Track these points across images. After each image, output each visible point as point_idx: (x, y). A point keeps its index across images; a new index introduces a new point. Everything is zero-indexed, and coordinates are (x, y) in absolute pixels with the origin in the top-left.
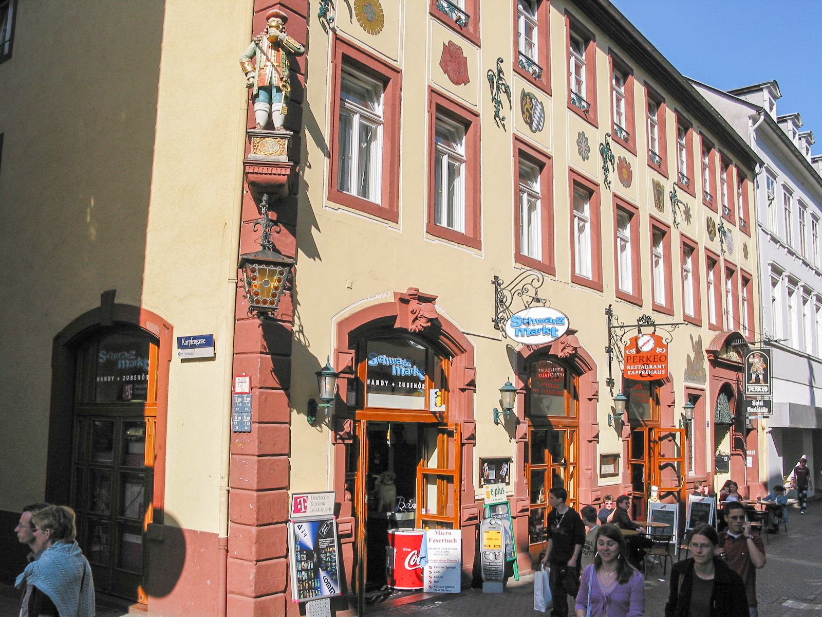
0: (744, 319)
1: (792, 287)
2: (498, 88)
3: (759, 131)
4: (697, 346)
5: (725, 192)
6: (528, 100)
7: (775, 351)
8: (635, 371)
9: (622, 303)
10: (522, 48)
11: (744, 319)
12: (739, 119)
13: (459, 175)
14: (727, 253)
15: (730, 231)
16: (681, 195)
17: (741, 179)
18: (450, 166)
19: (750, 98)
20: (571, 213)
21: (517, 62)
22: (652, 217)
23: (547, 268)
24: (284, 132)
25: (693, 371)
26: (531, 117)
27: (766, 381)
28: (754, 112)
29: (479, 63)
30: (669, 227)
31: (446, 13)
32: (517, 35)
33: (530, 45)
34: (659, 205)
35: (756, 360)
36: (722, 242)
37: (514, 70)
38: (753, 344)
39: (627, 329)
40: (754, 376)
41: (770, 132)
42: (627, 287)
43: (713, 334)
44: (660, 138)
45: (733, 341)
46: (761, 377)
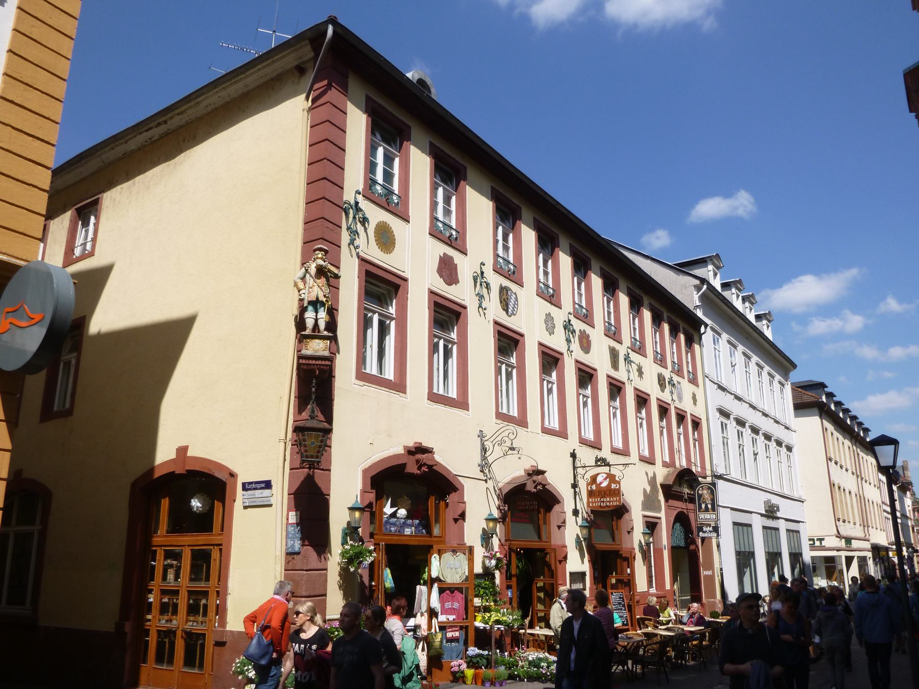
0: (695, 457)
1: (755, 436)
3: (703, 298)
4: (652, 481)
5: (690, 360)
7: (720, 483)
8: (597, 502)
9: (584, 447)
10: (440, 214)
11: (695, 457)
13: (452, 356)
14: (677, 402)
15: (679, 383)
16: (634, 356)
17: (690, 342)
18: (445, 347)
19: (699, 272)
20: (577, 391)
21: (496, 262)
22: (608, 376)
23: (521, 421)
24: (326, 333)
25: (649, 502)
26: (507, 305)
27: (713, 509)
28: (697, 282)
29: (465, 266)
30: (624, 383)
31: (441, 232)
32: (496, 242)
34: (615, 365)
35: (705, 492)
36: (672, 393)
37: (430, 234)
38: (705, 478)
40: (703, 506)
41: (714, 300)
42: (590, 435)
43: (665, 471)
45: (686, 477)
46: (709, 506)
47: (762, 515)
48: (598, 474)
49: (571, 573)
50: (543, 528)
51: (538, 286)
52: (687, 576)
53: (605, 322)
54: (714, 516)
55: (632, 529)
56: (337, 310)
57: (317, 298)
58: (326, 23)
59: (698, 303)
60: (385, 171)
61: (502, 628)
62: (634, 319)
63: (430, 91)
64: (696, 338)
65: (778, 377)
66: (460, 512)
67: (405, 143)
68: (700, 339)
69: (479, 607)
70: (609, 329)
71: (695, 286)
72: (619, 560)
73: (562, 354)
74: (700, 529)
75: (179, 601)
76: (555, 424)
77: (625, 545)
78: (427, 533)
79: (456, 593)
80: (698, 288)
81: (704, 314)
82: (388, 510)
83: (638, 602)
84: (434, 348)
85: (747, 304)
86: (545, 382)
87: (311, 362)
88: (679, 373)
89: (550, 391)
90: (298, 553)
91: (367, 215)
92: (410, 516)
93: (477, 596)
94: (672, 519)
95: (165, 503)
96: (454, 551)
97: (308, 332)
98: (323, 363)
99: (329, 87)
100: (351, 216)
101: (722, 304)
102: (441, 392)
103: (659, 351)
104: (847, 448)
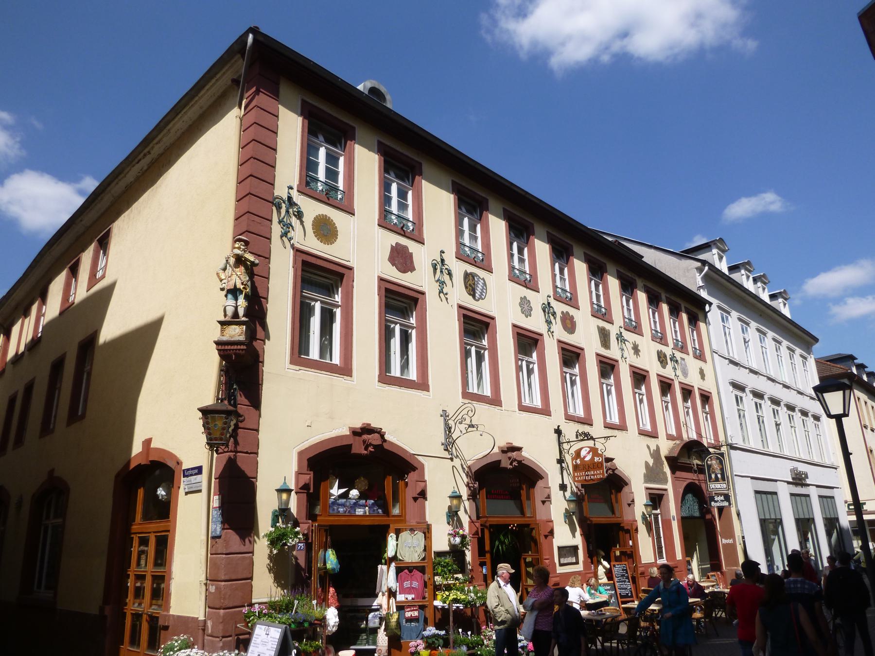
2: (441, 272)
3: (706, 278)
4: (656, 454)
6: (471, 278)
12: (686, 273)
13: (314, 315)
15: (684, 359)
17: (694, 321)
19: (702, 257)
20: (600, 381)
24: (244, 319)
25: (652, 474)
28: (699, 264)
32: (511, 256)
33: (521, 260)
35: (714, 462)
37: (379, 225)
39: (572, 444)
40: (713, 476)
43: (671, 443)
44: (604, 294)
45: (694, 448)
46: (719, 476)
47: (789, 483)
48: (582, 448)
49: (559, 548)
50: (526, 504)
51: (592, 308)
52: (705, 545)
53: (652, 330)
54: (725, 486)
55: (633, 501)
56: (266, 299)
57: (235, 285)
58: (246, 35)
59: (701, 284)
60: (327, 169)
61: (461, 607)
62: (674, 324)
63: (384, 99)
64: (701, 316)
65: (798, 351)
66: (419, 490)
67: (349, 142)
68: (706, 317)
69: (440, 585)
70: (599, 310)
71: (697, 269)
72: (621, 532)
73: (617, 361)
74: (712, 499)
75: (145, 585)
76: (615, 420)
77: (627, 517)
78: (384, 512)
79: (416, 572)
80: (700, 270)
81: (709, 294)
82: (336, 491)
83: (642, 573)
84: (519, 369)
85: (759, 284)
86: (604, 386)
87: (226, 347)
88: (683, 349)
89: (641, 401)
90: (219, 537)
91: (302, 210)
92: (362, 496)
93: (437, 574)
94: (681, 490)
95: (141, 492)
96: (412, 530)
97: (228, 319)
98: (239, 347)
99: (257, 92)
100: (283, 211)
101: (729, 284)
102: (475, 391)
103: (697, 347)
104: (863, 403)
